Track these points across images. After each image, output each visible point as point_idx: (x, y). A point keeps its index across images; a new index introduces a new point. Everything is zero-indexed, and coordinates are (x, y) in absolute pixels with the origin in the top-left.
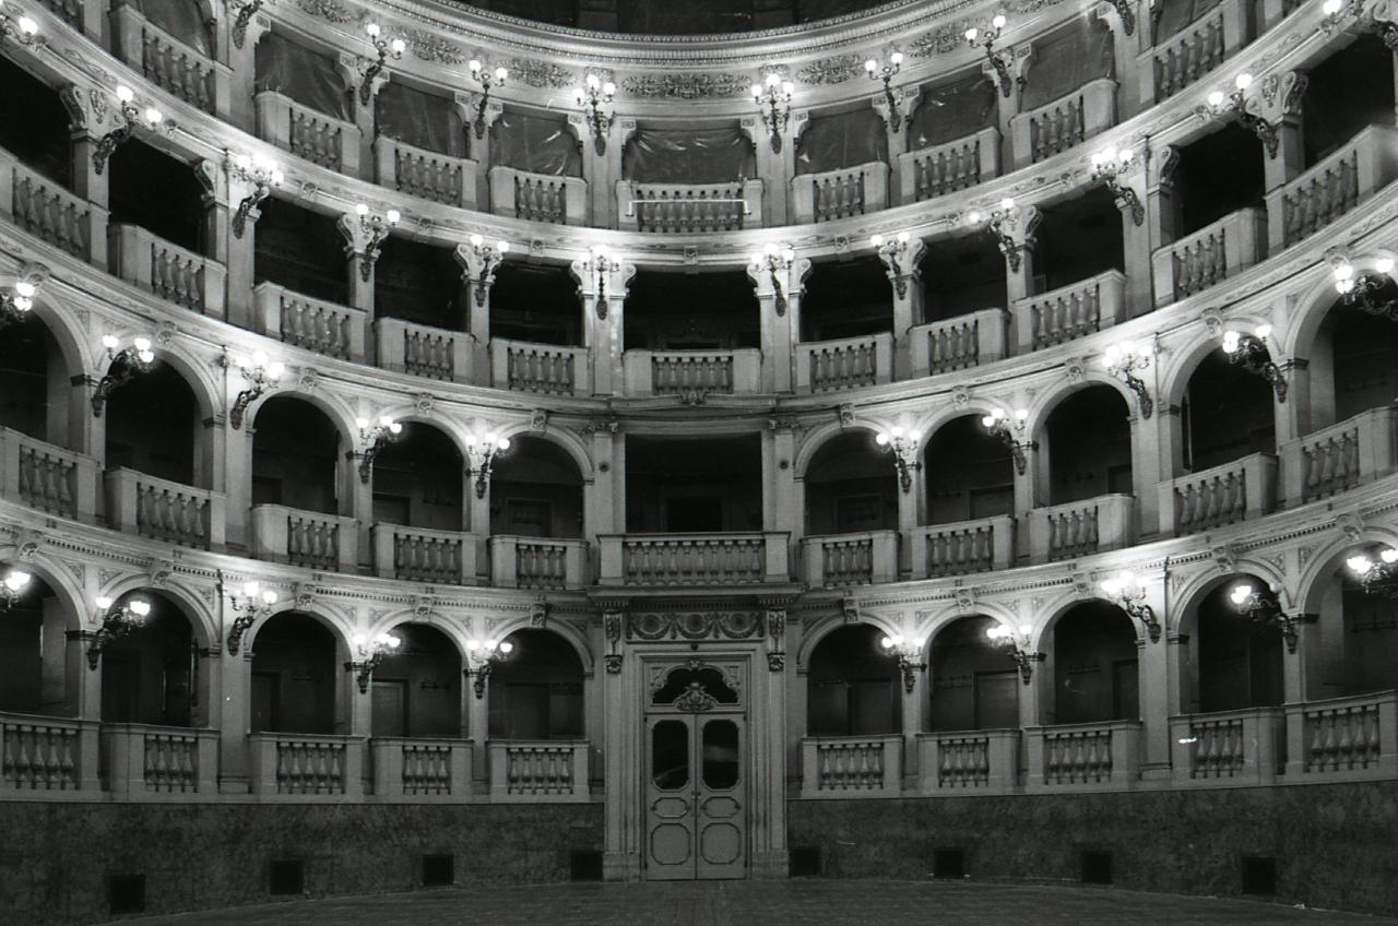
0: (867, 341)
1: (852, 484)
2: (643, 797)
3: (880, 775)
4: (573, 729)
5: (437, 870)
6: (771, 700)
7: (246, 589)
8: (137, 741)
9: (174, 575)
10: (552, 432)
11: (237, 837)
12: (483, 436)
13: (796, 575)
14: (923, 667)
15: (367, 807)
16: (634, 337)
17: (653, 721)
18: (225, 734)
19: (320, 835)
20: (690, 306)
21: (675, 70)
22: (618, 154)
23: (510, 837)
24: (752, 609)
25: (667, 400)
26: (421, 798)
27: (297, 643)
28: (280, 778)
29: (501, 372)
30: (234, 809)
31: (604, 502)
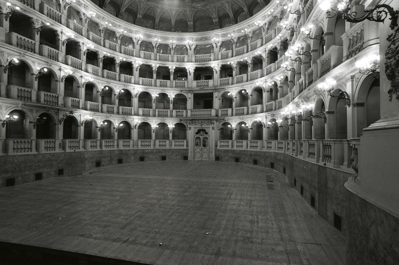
1: (227, 101)
2: (194, 149)
5: (164, 158)
6: (213, 133)
8: (122, 141)
9: (127, 119)
10: (182, 93)
11: (135, 154)
12: (172, 95)
13: (217, 115)
15: (154, 149)
17: (196, 137)
18: (134, 140)
19: (147, 153)
20: (203, 73)
21: (202, 36)
22: (193, 50)
23: (174, 154)
24: (210, 121)
25: (198, 88)
26: (162, 148)
27: (145, 126)
28: (141, 145)
29: (174, 86)
30: (135, 150)
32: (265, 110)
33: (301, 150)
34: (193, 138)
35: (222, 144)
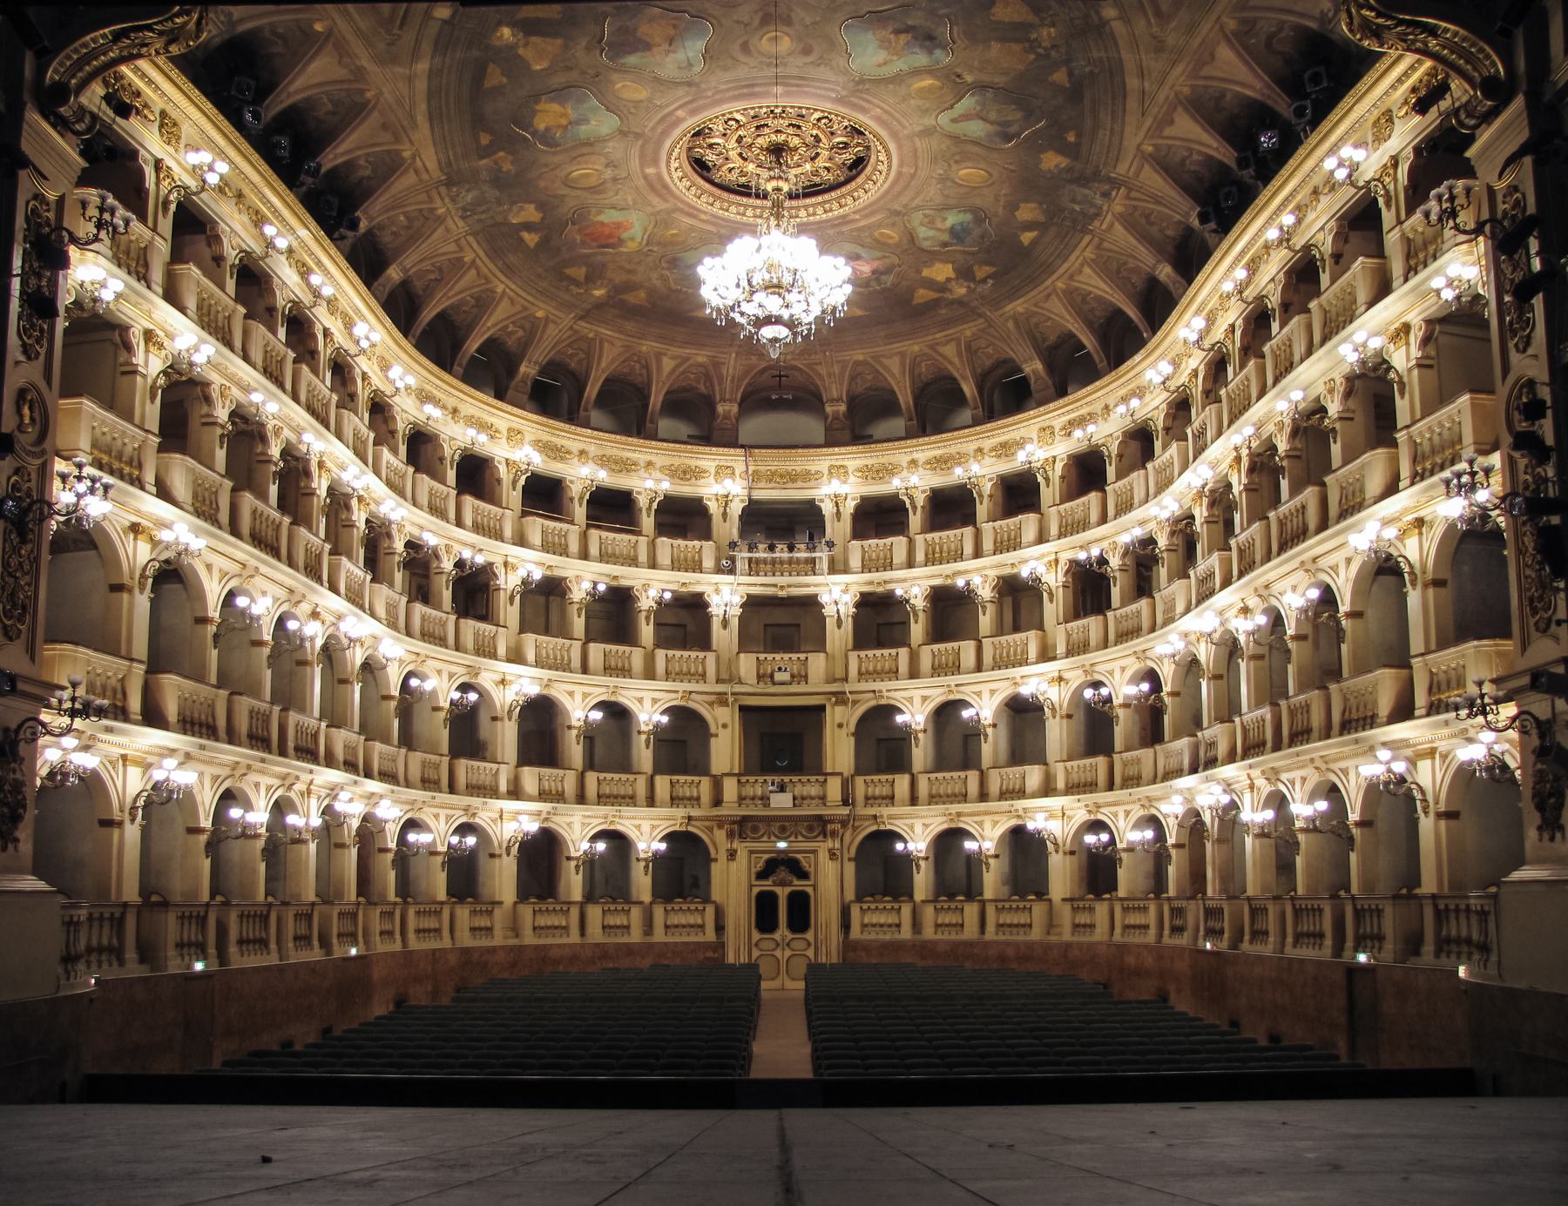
0: (893, 651)
1: (883, 744)
3: (898, 926)
4: (707, 899)
6: (831, 877)
7: (513, 821)
14: (926, 859)
16: (746, 642)
17: (756, 890)
20: (782, 623)
24: (819, 826)
28: (667, 927)
30: (512, 948)
31: (725, 750)
32: (1061, 784)
33: (1258, 926)
34: (744, 897)
35: (871, 918)
